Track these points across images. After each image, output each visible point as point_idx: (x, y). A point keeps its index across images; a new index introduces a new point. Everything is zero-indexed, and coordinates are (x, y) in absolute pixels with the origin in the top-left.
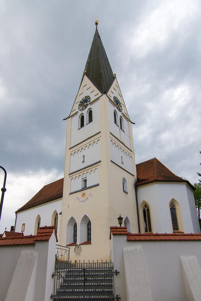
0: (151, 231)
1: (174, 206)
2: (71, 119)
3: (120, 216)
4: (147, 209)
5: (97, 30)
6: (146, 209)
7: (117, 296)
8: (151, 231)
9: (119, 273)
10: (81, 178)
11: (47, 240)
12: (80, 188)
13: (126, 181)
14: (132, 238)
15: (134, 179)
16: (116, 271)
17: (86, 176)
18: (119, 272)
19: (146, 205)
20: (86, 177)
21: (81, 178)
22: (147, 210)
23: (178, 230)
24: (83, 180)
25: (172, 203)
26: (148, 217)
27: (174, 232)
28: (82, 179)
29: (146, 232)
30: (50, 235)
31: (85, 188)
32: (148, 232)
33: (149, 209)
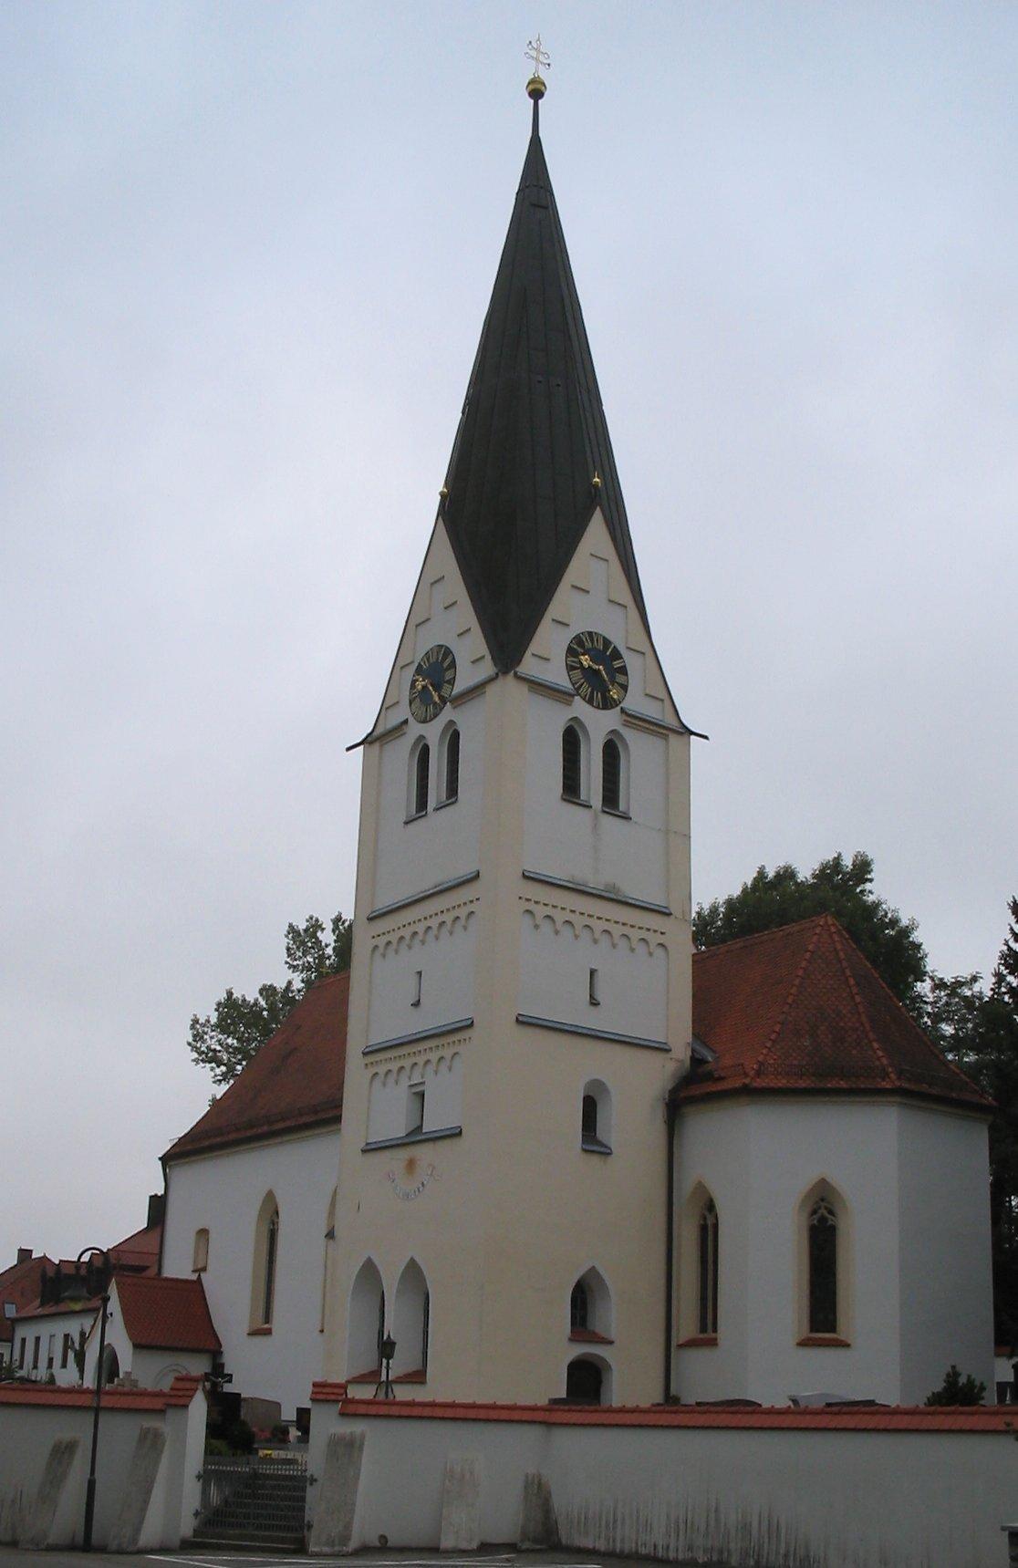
1: (831, 1212)
2: (381, 758)
5: (535, 145)
7: (309, 1522)
9: (316, 1480)
10: (405, 1083)
11: (186, 1406)
12: (400, 1131)
14: (351, 1408)
16: (312, 1476)
17: (422, 1078)
20: (423, 1083)
21: (405, 1083)
24: (414, 1093)
25: (822, 1200)
28: (411, 1086)
30: (192, 1397)
31: (416, 1137)
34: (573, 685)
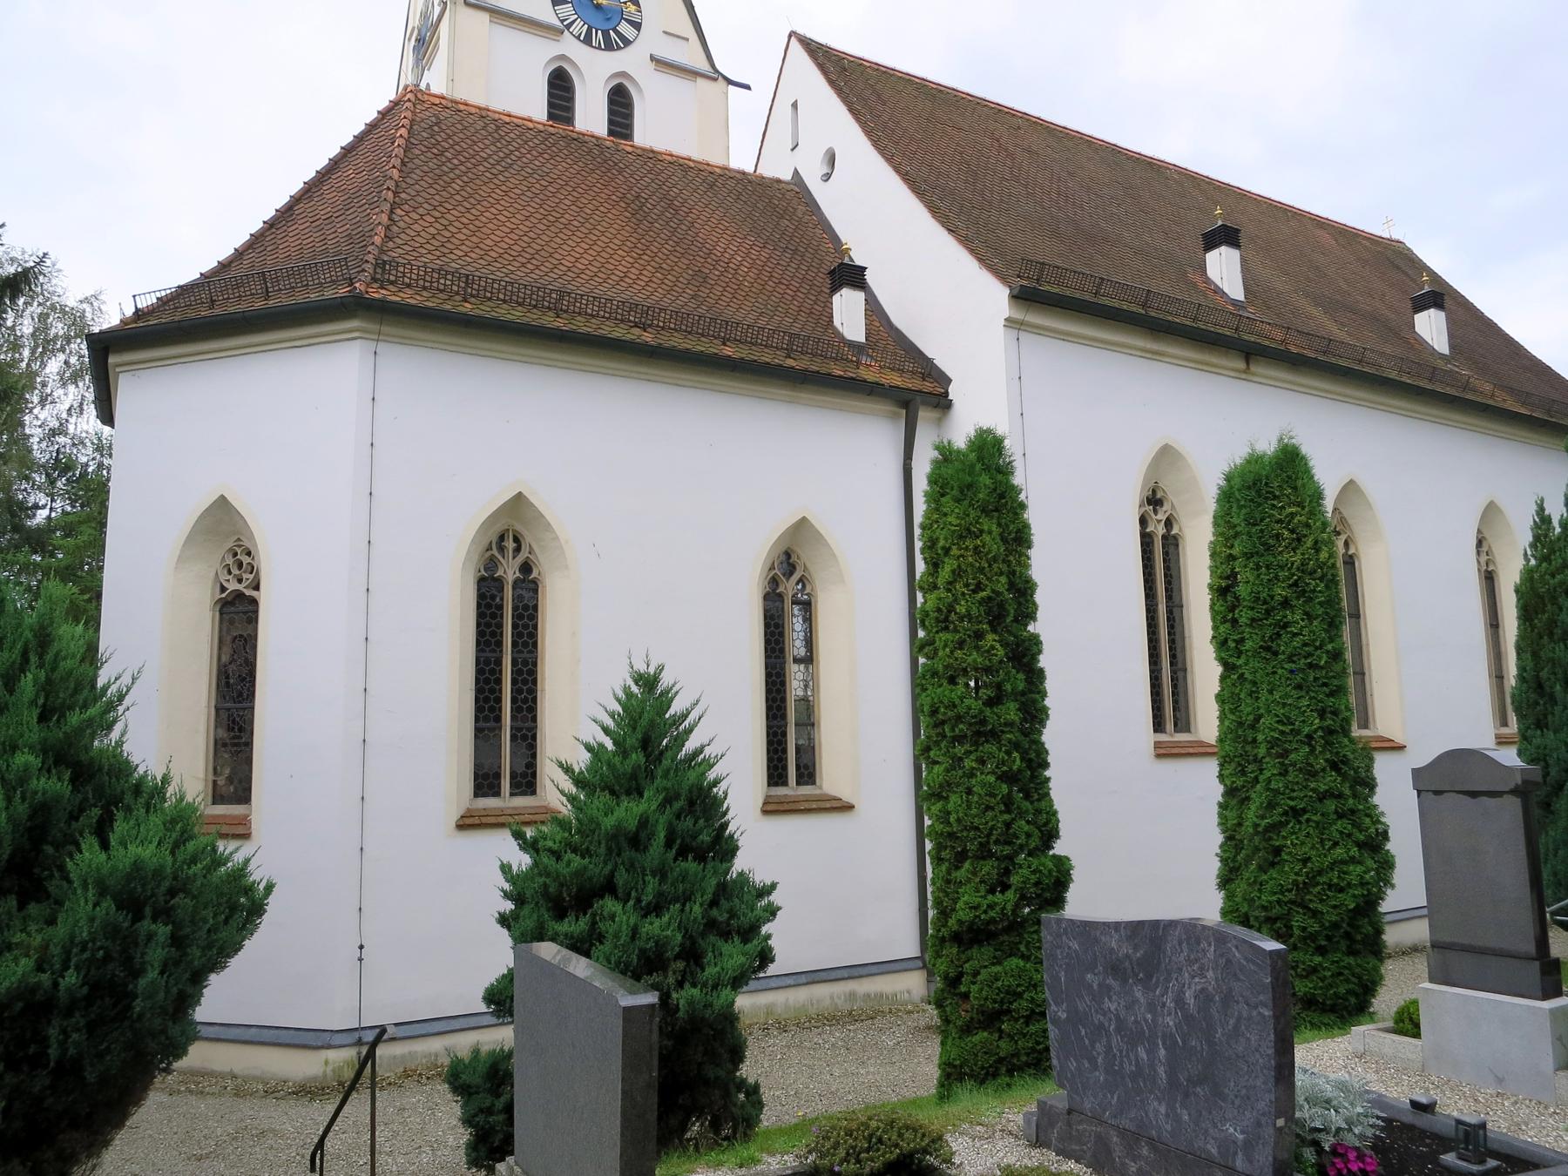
34: (562, 21)
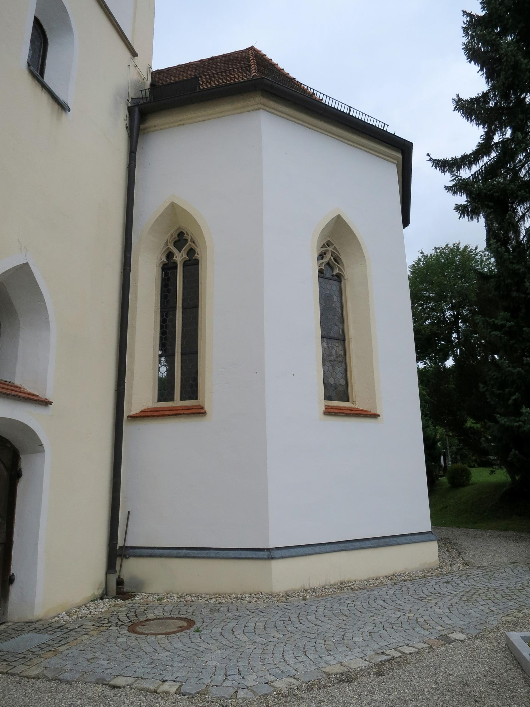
0: (196, 398)
1: (337, 259)
3: (428, 160)
4: (185, 256)
6: (180, 257)
8: (196, 398)
13: (43, 451)
15: (133, 75)
18: (138, 55)
19: (181, 234)
22: (185, 264)
23: (348, 401)
25: (328, 244)
26: (183, 308)
27: (332, 408)
29: (159, 400)
32: (172, 399)
33: (196, 263)
